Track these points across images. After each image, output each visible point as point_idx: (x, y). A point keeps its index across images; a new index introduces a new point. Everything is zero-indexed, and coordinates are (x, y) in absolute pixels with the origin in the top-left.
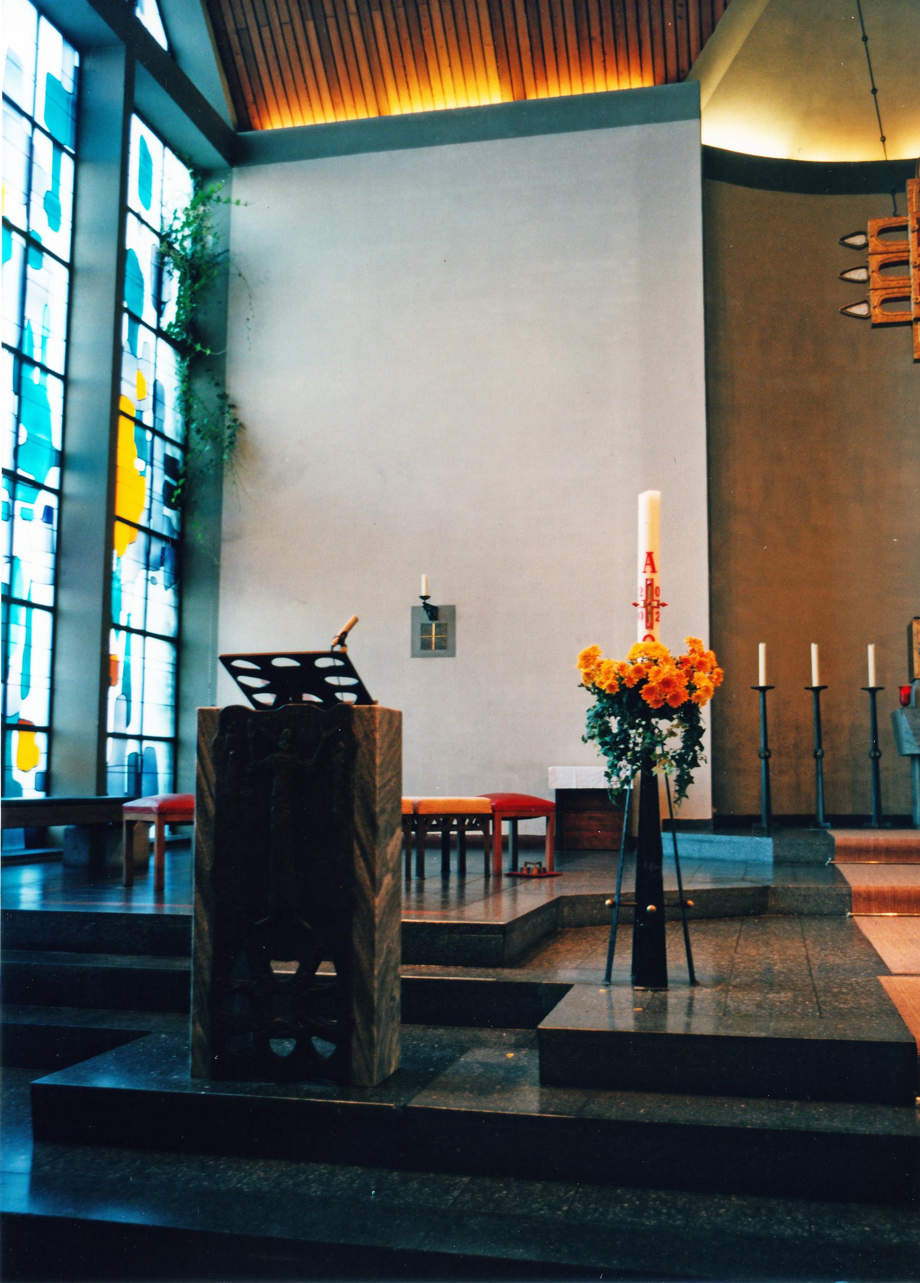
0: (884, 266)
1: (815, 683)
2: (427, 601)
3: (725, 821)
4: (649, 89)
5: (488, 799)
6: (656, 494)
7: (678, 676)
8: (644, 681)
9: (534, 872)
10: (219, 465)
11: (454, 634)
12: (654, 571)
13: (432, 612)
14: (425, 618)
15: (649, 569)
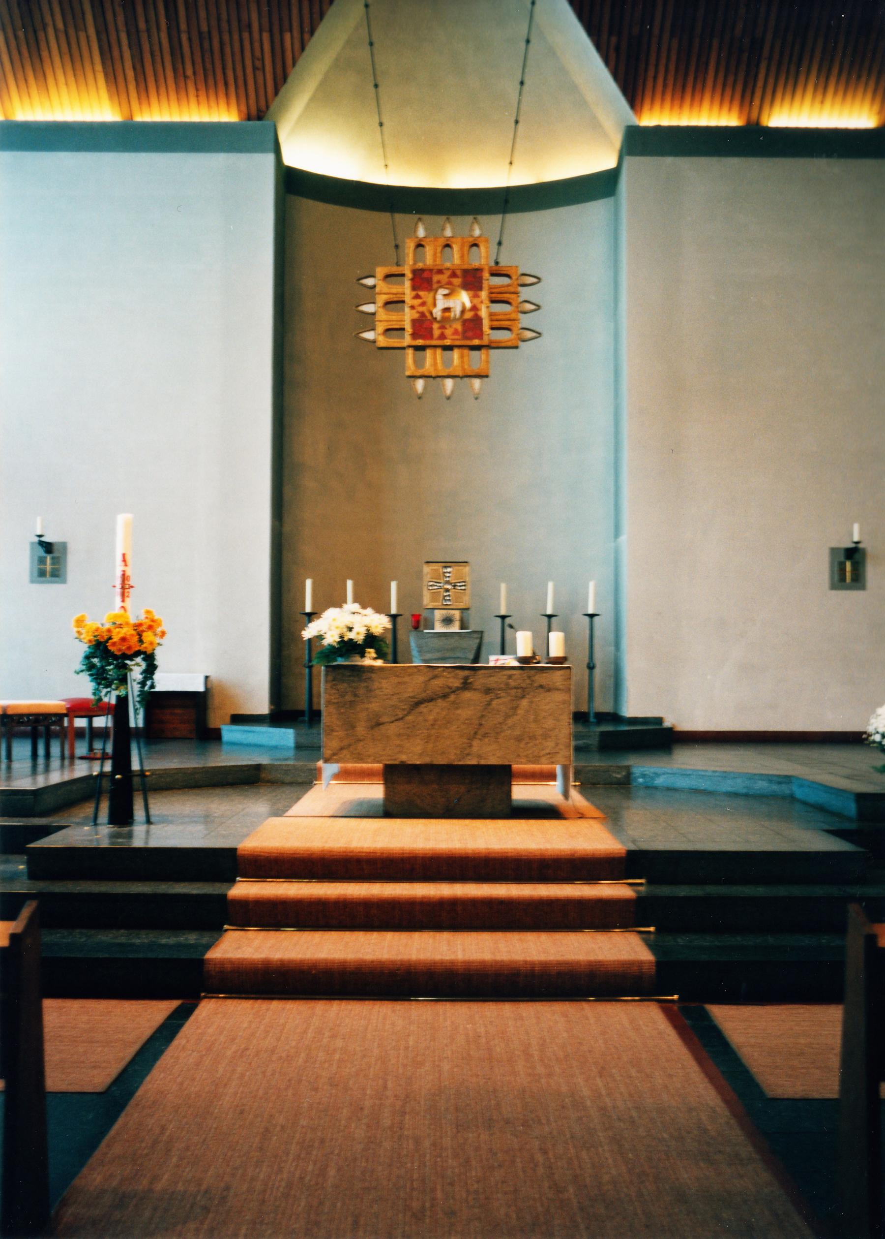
0: (387, 303)
2: (43, 539)
4: (234, 123)
5: (63, 703)
6: (129, 516)
7: (132, 635)
8: (110, 638)
9: (99, 755)
11: (65, 566)
12: (126, 565)
13: (48, 547)
14: (41, 552)
15: (123, 563)
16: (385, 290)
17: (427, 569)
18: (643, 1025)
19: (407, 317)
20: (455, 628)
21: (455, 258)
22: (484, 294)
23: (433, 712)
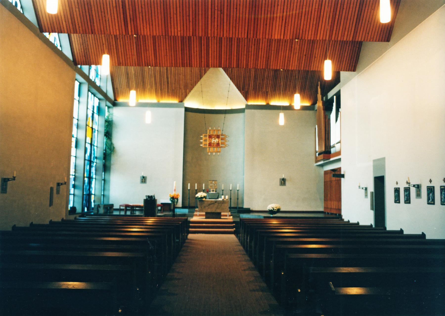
1: (196, 189)
3: (184, 207)
10: (111, 153)
13: (143, 177)
16: (204, 138)
17: (209, 182)
18: (233, 236)
19: (208, 142)
20: (214, 192)
21: (215, 133)
22: (220, 139)
23: (211, 206)
